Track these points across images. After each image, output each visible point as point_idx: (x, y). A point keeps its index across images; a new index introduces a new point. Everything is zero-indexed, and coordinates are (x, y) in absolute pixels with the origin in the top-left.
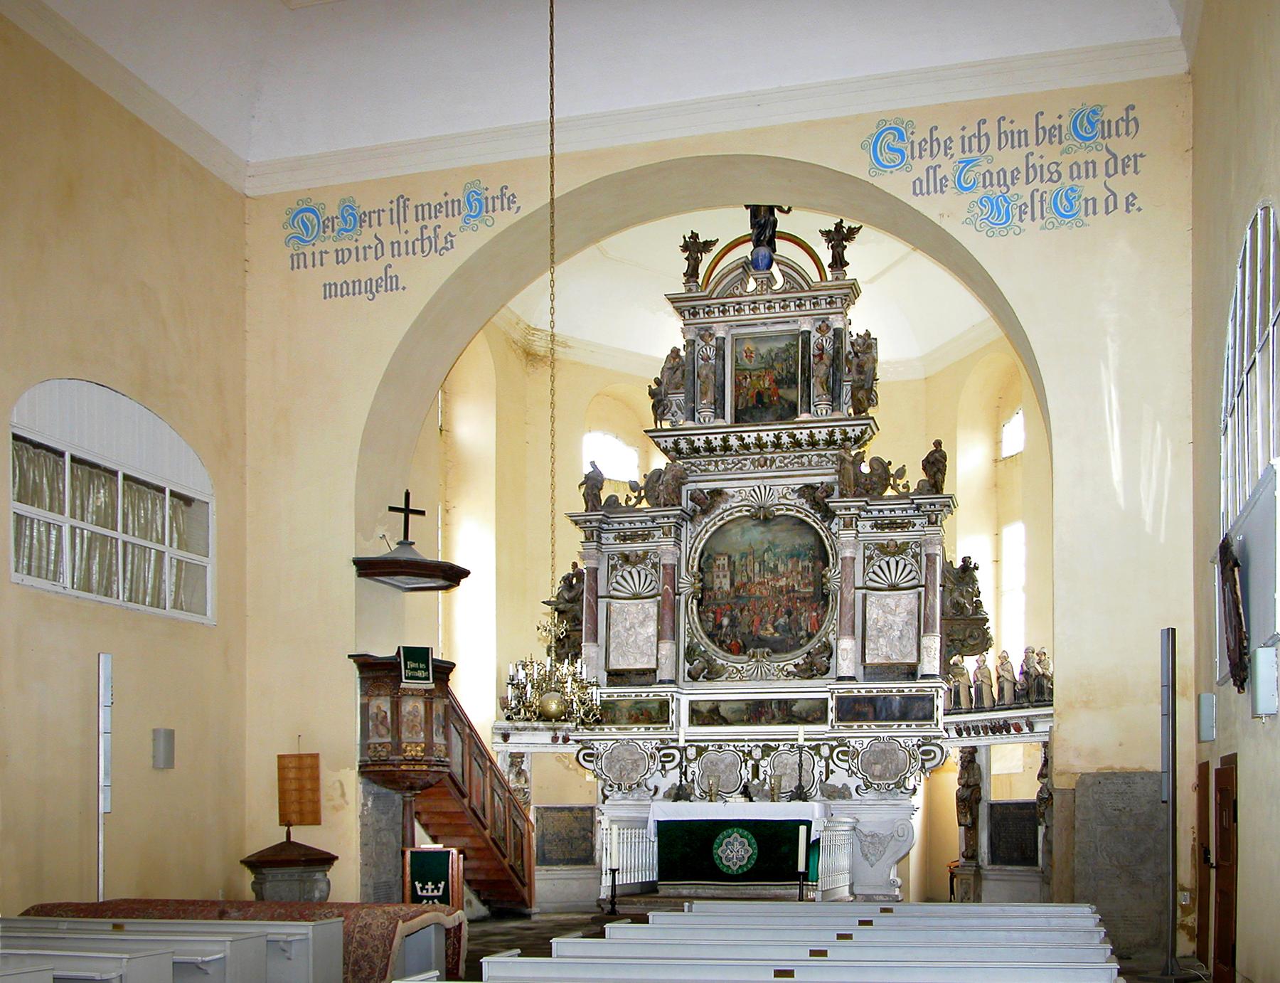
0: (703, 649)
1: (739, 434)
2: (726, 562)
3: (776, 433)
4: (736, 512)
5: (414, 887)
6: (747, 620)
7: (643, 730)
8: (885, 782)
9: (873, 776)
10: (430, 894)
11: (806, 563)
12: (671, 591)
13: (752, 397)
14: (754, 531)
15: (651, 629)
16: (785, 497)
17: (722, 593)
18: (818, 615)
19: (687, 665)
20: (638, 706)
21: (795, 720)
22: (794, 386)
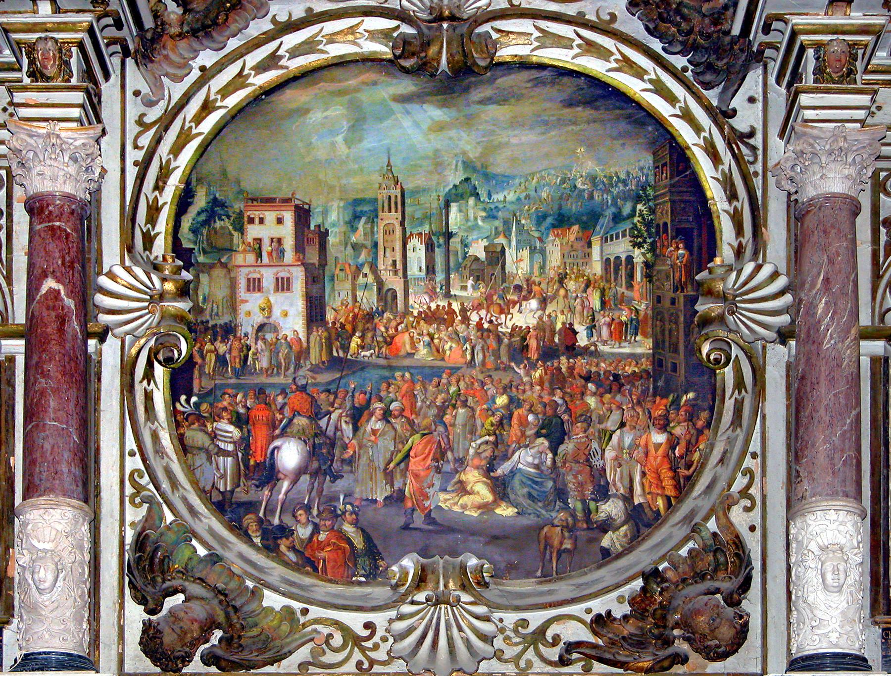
0: (202, 552)
2: (287, 231)
11: (621, 248)
12: (70, 303)
14: (407, 123)
17: (273, 348)
18: (672, 444)
19: (136, 614)
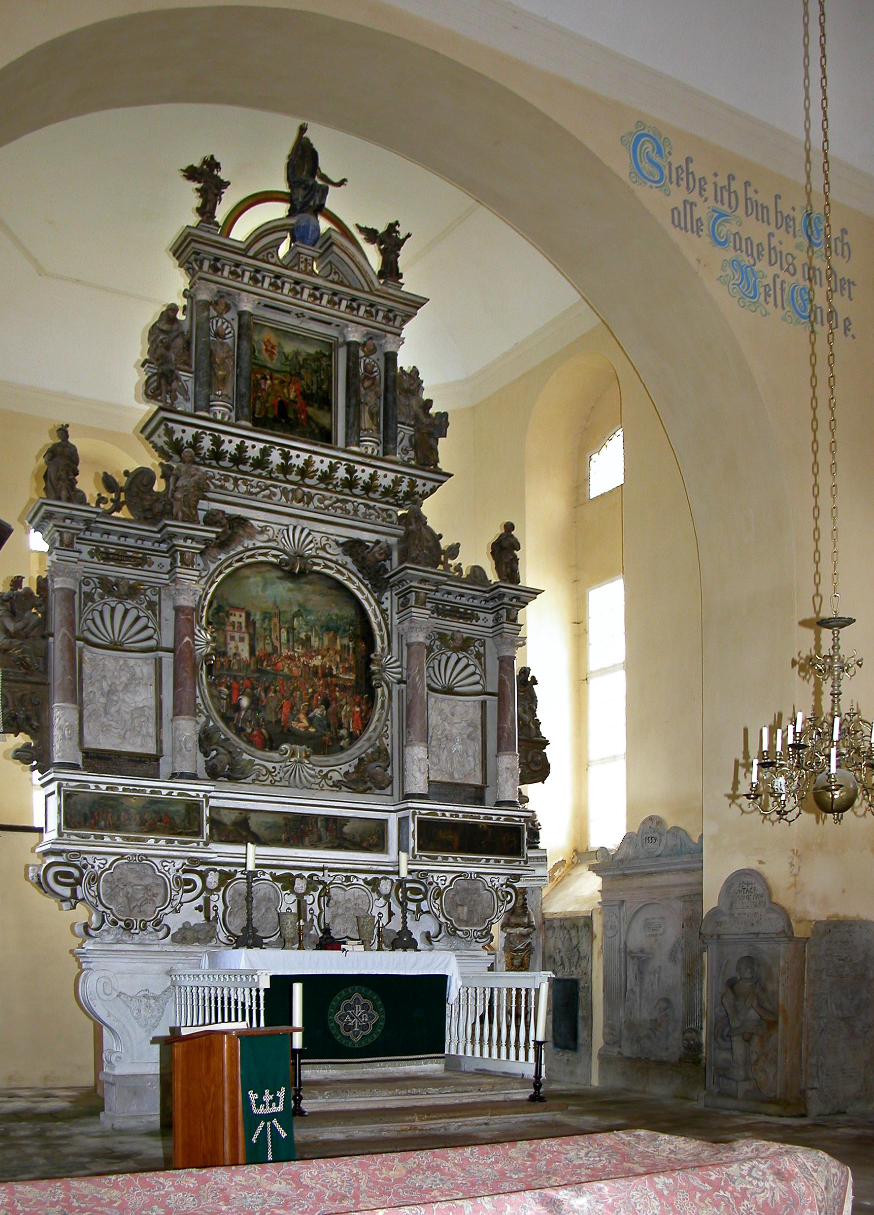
1: (286, 450)
2: (243, 620)
3: (334, 461)
4: (261, 554)
5: (246, 1099)
6: (273, 704)
7: (162, 842)
8: (474, 928)
9: (459, 920)
10: (268, 1110)
11: (346, 641)
13: (273, 406)
14: (281, 587)
15: (144, 697)
16: (323, 549)
18: (361, 711)
20: (154, 807)
21: (346, 844)
22: (326, 408)
